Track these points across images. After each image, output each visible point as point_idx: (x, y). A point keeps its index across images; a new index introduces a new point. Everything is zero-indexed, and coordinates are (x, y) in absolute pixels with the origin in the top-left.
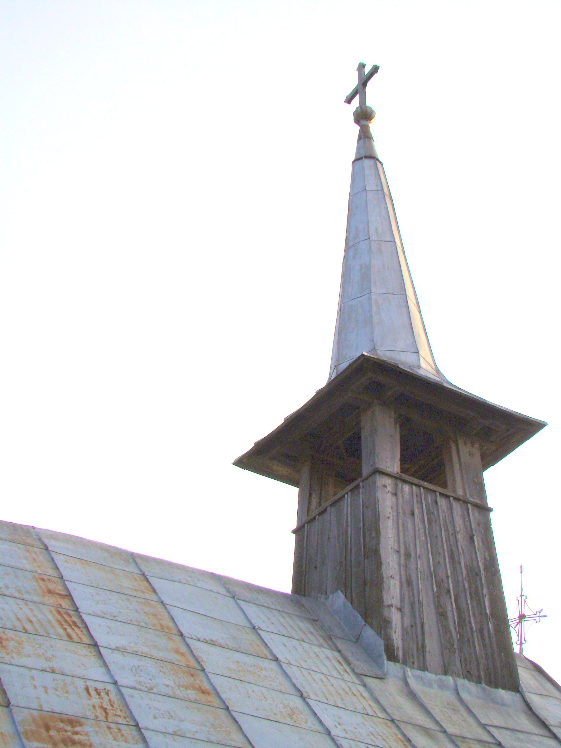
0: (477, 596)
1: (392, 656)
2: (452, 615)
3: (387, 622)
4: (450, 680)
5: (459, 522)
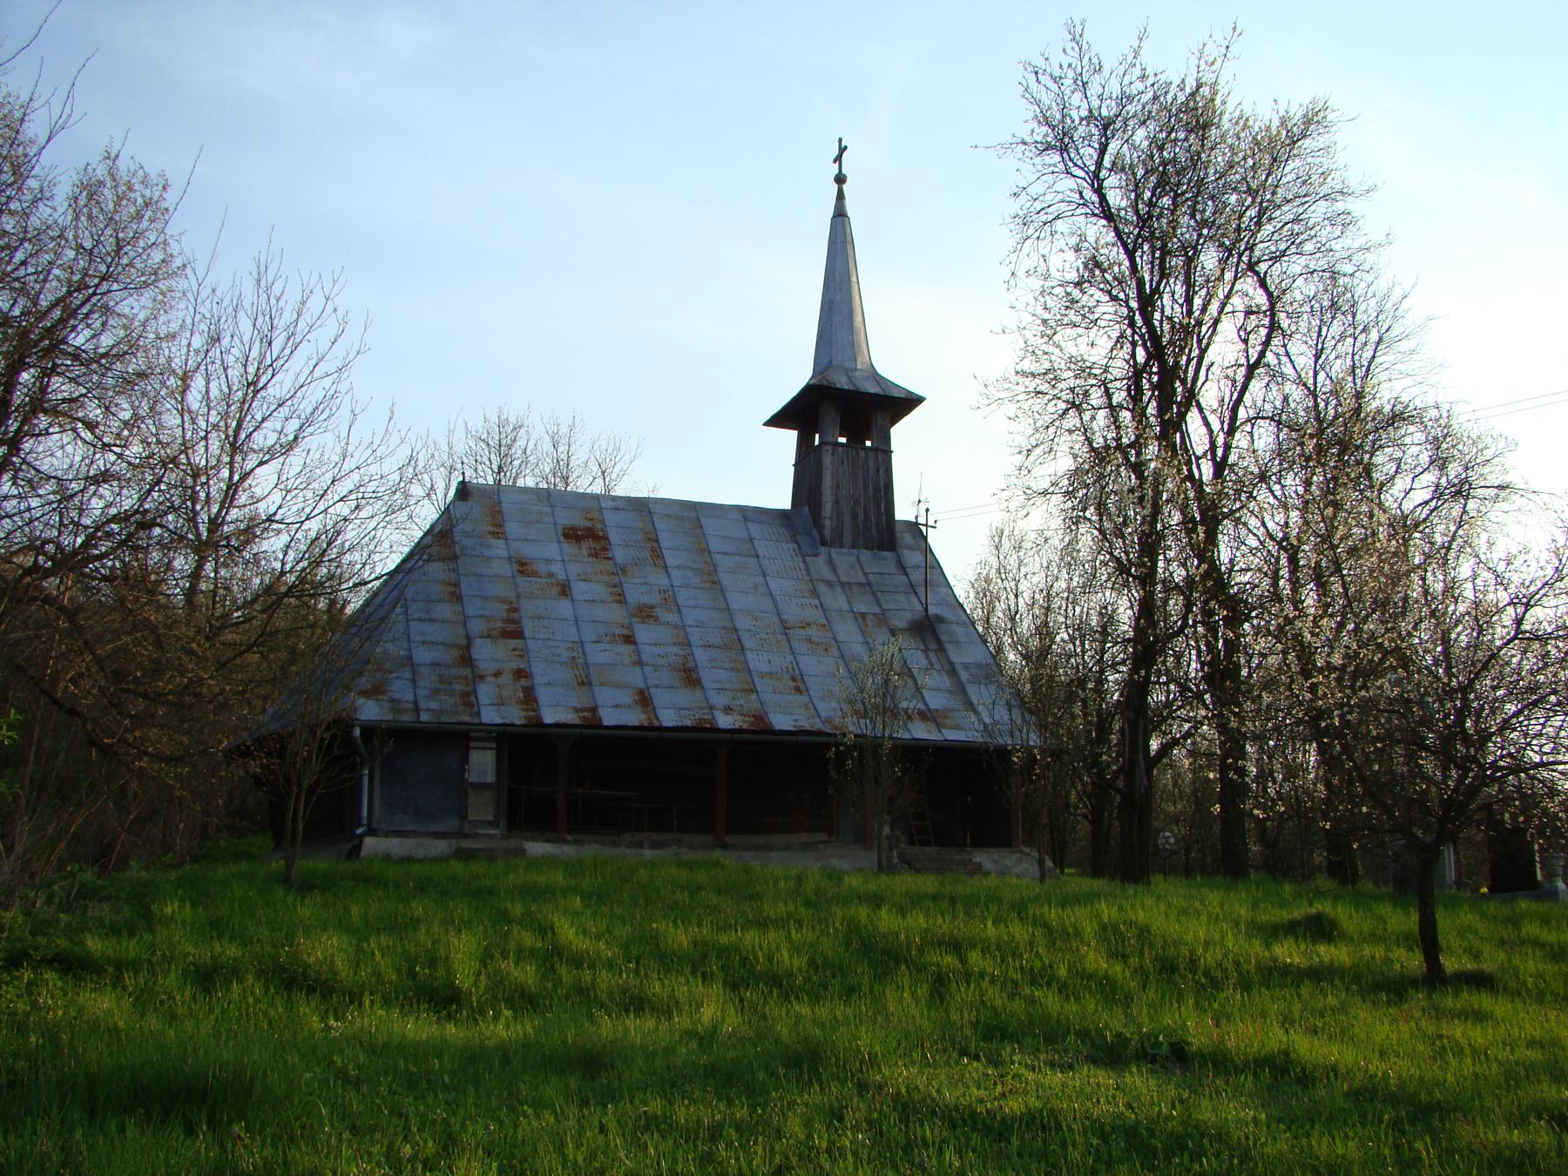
0: (877, 505)
1: (823, 543)
2: (861, 517)
3: (823, 526)
4: (855, 551)
5: (871, 464)
